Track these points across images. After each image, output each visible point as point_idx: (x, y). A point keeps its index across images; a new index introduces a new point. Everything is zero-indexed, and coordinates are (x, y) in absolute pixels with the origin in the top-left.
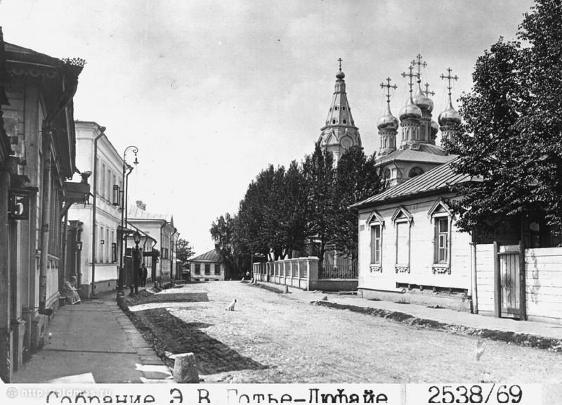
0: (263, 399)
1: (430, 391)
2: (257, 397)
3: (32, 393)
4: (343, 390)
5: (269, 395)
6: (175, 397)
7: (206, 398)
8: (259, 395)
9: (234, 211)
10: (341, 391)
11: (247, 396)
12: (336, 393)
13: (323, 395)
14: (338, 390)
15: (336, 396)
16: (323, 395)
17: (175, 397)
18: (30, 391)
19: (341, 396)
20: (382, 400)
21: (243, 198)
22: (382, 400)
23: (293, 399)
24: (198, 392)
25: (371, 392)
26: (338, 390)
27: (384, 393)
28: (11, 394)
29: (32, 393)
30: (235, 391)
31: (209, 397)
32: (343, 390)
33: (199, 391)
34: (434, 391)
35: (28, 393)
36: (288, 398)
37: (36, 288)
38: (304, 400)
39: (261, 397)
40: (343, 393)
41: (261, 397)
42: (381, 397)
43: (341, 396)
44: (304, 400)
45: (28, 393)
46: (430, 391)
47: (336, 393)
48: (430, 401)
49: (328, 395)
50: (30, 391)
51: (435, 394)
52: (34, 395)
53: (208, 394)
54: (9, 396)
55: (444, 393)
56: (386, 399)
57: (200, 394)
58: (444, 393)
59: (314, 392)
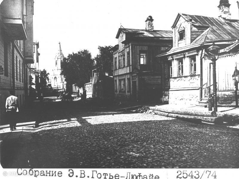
0: (107, 175)
1: (178, 172)
2: (104, 175)
3: (14, 174)
4: (141, 173)
5: (110, 174)
6: (70, 173)
7: (84, 174)
8: (105, 174)
9: (216, 61)
10: (140, 174)
11: (100, 174)
12: (137, 175)
13: (132, 175)
14: (139, 173)
15: (138, 176)
16: (132, 175)
17: (70, 173)
18: (13, 173)
19: (140, 176)
20: (157, 178)
21: (76, 52)
22: (157, 178)
23: (120, 176)
24: (80, 171)
25: (152, 175)
26: (139, 173)
27: (159, 176)
28: (5, 174)
29: (14, 174)
30: (96, 172)
31: (85, 174)
32: (141, 173)
33: (81, 171)
34: (179, 173)
35: (12, 174)
36: (118, 176)
37: (20, 123)
38: (121, 177)
39: (106, 175)
40: (140, 175)
41: (106, 175)
42: (157, 177)
43: (140, 176)
44: (121, 177)
45: (12, 174)
46: (178, 172)
47: (137, 175)
48: (177, 177)
49: (134, 175)
50: (13, 173)
51: (180, 174)
52: (15, 175)
53: (84, 173)
54: (4, 175)
55: (183, 174)
56: (159, 178)
57: (81, 175)
58: (183, 174)
59: (129, 174)
